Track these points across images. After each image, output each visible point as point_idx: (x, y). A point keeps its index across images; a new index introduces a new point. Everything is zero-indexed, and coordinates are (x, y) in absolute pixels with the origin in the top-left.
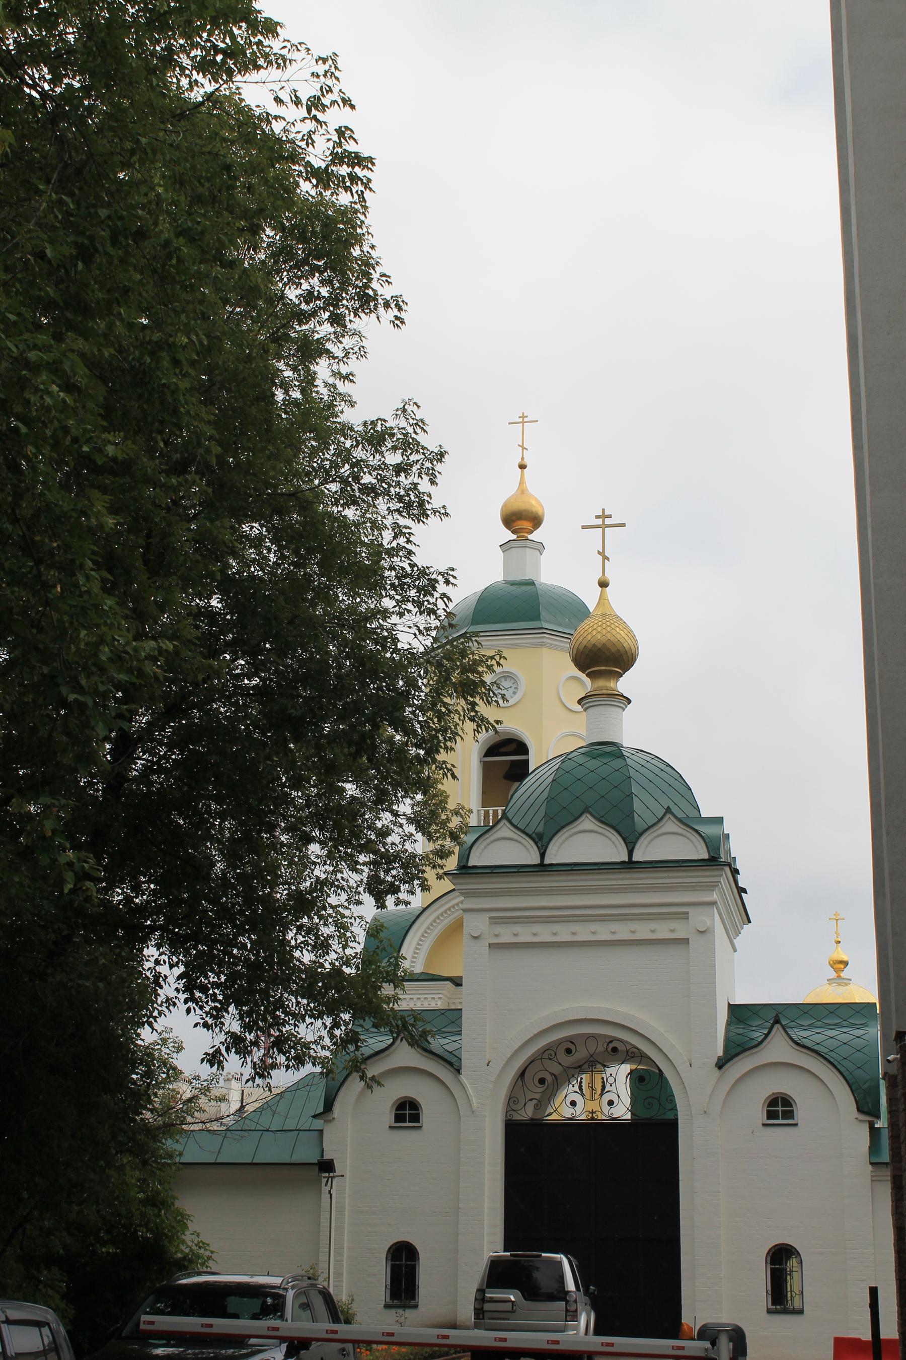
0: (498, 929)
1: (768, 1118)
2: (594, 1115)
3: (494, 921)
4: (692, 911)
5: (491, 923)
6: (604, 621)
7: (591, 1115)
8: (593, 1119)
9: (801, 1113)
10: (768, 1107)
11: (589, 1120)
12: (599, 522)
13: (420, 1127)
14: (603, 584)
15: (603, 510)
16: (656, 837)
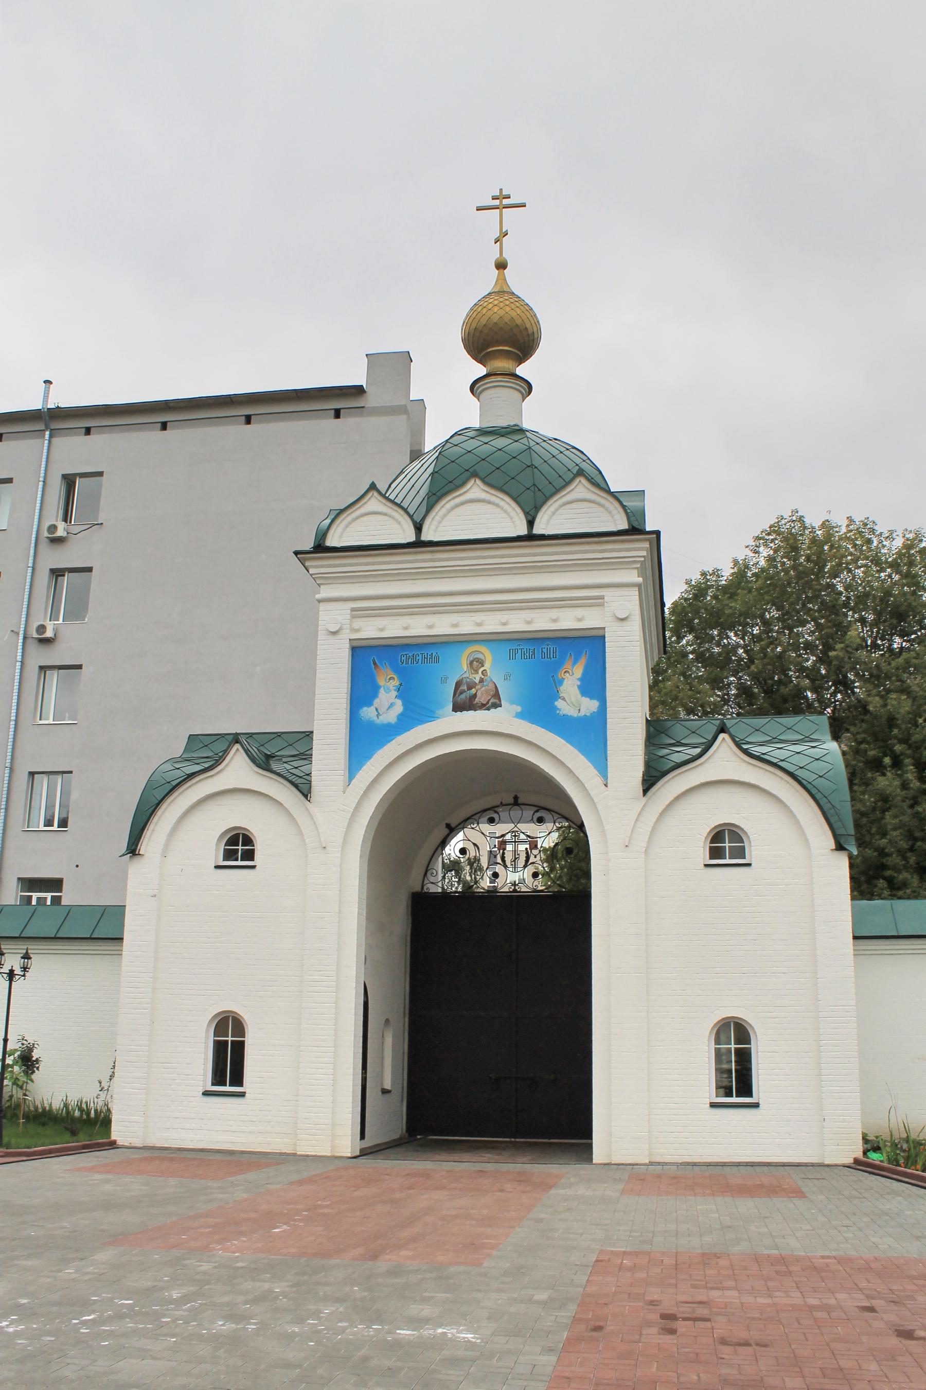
0: (357, 623)
1: (711, 858)
2: (517, 887)
3: (357, 613)
4: (607, 593)
7: (513, 888)
8: (515, 891)
9: (754, 852)
10: (711, 843)
11: (510, 892)
12: (497, 202)
13: (253, 867)
14: (501, 266)
15: (501, 190)
16: (458, 506)
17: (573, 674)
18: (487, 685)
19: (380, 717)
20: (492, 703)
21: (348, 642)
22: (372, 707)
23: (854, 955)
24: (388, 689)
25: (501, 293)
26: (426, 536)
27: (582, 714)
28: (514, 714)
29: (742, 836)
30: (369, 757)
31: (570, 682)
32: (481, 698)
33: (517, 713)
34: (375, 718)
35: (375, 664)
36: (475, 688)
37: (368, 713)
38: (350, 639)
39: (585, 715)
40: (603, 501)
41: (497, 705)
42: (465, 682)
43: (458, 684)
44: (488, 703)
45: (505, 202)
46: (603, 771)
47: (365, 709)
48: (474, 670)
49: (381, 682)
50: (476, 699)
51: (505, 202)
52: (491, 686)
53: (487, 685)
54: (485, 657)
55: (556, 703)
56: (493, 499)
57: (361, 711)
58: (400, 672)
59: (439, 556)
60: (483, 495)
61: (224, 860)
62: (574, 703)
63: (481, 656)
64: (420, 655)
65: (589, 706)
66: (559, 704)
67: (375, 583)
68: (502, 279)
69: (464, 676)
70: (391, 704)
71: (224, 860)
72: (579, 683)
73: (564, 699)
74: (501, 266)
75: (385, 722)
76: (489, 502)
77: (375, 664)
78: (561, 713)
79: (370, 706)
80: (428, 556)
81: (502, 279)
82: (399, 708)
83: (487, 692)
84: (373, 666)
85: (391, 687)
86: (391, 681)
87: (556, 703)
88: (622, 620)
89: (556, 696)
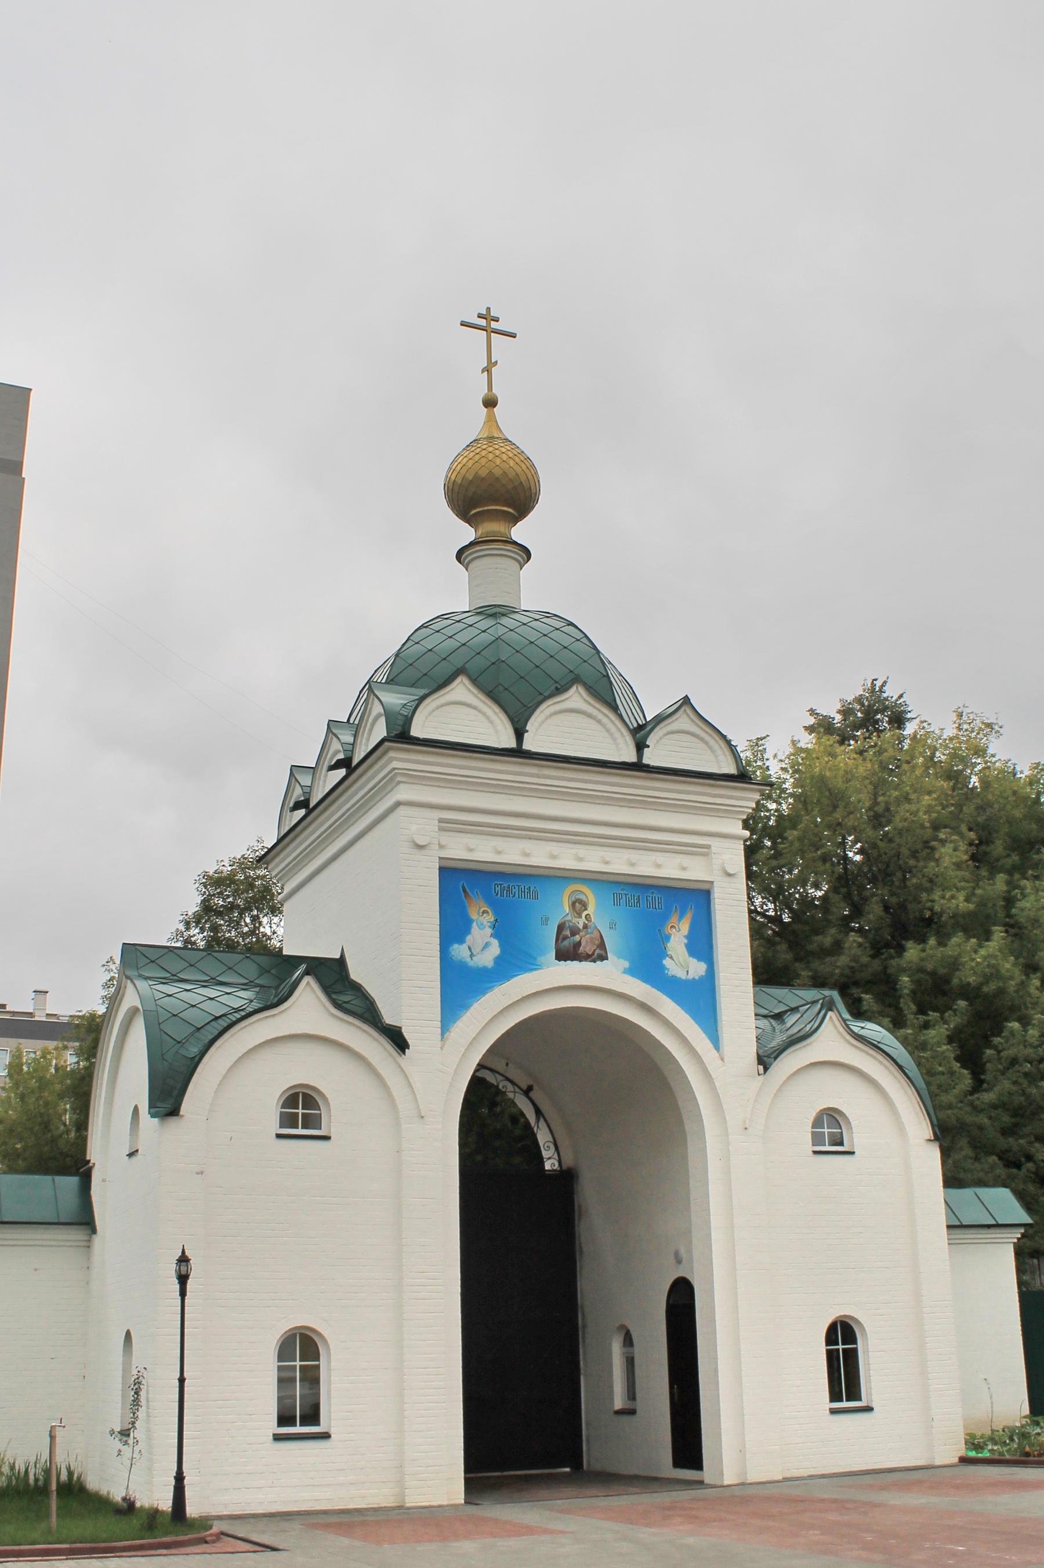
0: (446, 838)
4: (715, 844)
5: (441, 829)
6: (491, 449)
9: (333, 1121)
12: (483, 322)
14: (490, 403)
15: (488, 309)
17: (680, 930)
18: (592, 933)
19: (474, 958)
20: (598, 954)
21: (438, 861)
22: (464, 945)
23: (949, 1244)
24: (482, 924)
25: (491, 438)
26: (650, 758)
27: (690, 977)
28: (623, 970)
29: (320, 1104)
30: (466, 1007)
31: (677, 939)
32: (586, 948)
33: (625, 968)
34: (468, 959)
35: (464, 891)
36: (579, 934)
37: (459, 951)
38: (440, 858)
39: (693, 978)
40: (707, 738)
41: (603, 958)
42: (567, 925)
43: (561, 928)
44: (593, 954)
45: (494, 325)
46: (715, 1040)
47: (456, 946)
48: (577, 913)
49: (474, 915)
50: (581, 948)
51: (494, 325)
52: (596, 934)
53: (592, 933)
54: (588, 899)
55: (664, 962)
56: (595, 712)
57: (451, 948)
58: (495, 905)
59: (547, 772)
60: (585, 707)
61: (280, 1127)
62: (682, 962)
63: (583, 897)
64: (517, 888)
65: (697, 969)
66: (667, 962)
67: (601, 806)
68: (491, 420)
69: (566, 919)
70: (486, 944)
71: (280, 1127)
72: (686, 941)
73: (671, 958)
74: (490, 403)
75: (481, 964)
76: (590, 716)
77: (464, 891)
78: (669, 973)
79: (462, 944)
80: (534, 770)
81: (491, 420)
82: (495, 949)
83: (592, 940)
84: (463, 894)
85: (485, 923)
86: (485, 915)
87: (664, 962)
88: (730, 875)
89: (663, 953)
